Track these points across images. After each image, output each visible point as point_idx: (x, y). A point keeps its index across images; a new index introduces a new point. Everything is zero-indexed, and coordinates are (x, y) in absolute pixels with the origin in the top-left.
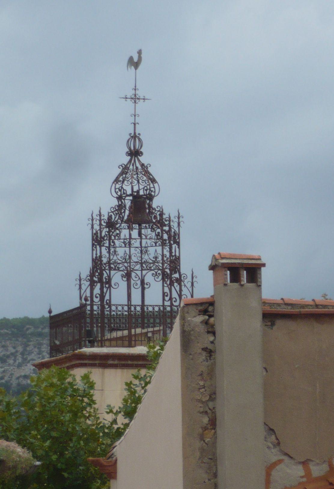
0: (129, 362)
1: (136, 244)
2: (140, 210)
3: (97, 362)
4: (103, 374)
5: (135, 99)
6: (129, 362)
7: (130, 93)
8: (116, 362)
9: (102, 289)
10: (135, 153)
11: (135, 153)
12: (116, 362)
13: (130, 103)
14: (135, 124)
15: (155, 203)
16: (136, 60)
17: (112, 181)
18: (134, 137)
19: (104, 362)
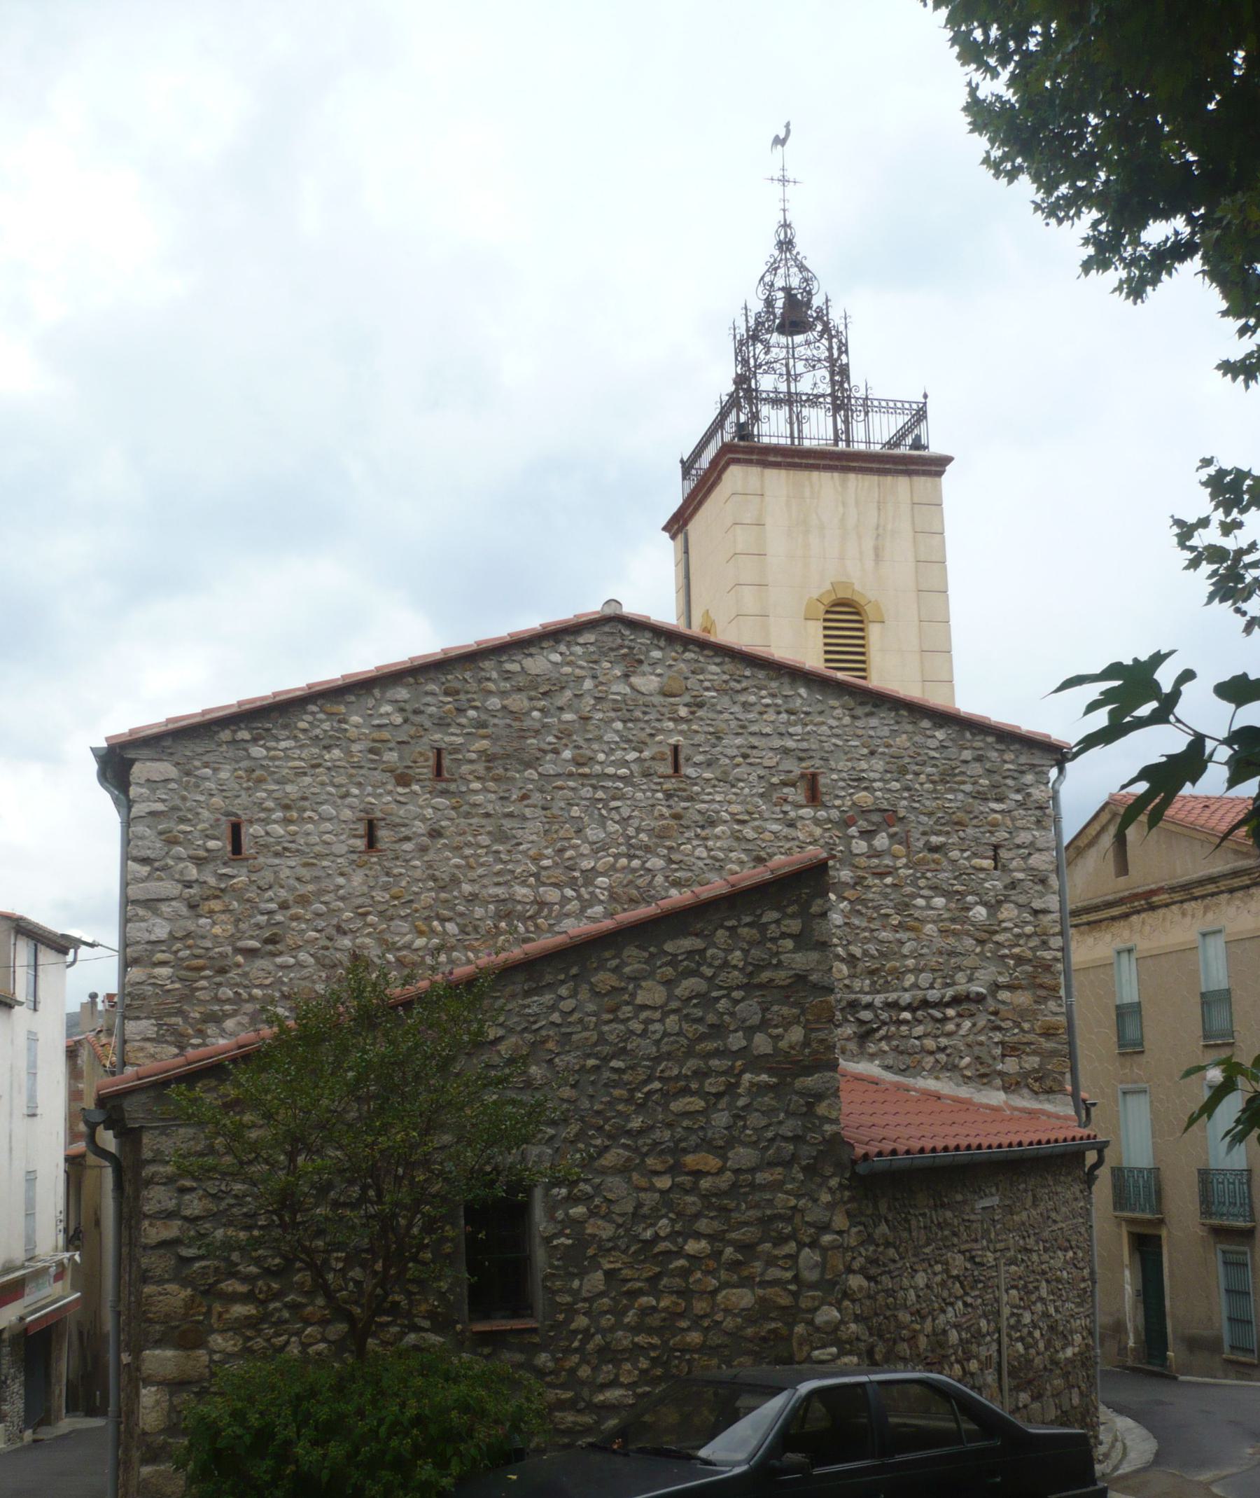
0: (797, 460)
1: (798, 364)
2: (795, 314)
3: (754, 457)
4: (762, 475)
5: (784, 181)
6: (797, 460)
7: (778, 174)
8: (779, 459)
9: (257, 986)
10: (786, 245)
11: (786, 245)
12: (779, 459)
13: (778, 186)
14: (784, 210)
15: (992, 172)
16: (782, 137)
17: (1078, 1023)
18: (786, 225)
19: (763, 458)
